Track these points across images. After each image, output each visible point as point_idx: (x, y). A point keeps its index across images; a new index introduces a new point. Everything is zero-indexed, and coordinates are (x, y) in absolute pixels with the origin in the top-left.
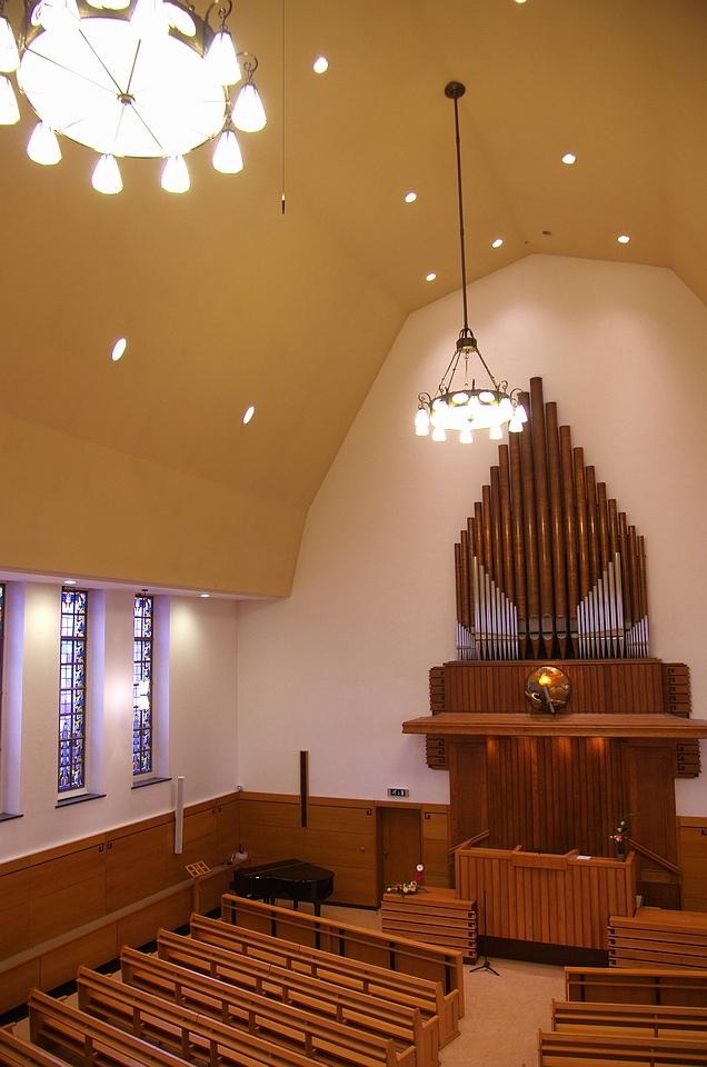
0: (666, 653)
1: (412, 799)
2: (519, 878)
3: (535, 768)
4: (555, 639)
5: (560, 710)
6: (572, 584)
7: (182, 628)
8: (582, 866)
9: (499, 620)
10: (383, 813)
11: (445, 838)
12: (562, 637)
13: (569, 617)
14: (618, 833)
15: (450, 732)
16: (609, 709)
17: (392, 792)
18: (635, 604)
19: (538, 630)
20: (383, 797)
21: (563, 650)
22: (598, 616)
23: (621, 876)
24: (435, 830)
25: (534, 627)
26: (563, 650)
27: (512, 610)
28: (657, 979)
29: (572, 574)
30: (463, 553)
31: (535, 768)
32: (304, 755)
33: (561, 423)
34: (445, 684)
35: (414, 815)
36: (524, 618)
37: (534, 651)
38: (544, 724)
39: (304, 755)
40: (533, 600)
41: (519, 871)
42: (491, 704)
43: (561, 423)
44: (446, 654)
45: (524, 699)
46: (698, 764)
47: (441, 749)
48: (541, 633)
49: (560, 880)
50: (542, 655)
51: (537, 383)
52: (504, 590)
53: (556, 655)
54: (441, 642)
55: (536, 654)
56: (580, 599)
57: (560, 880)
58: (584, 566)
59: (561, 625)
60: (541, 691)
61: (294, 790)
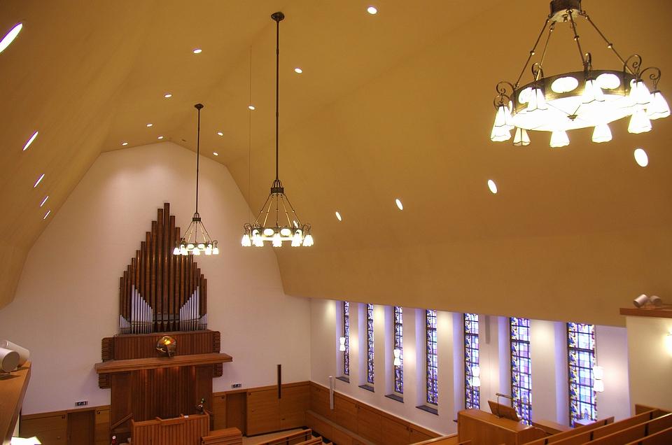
0: (212, 327)
1: (243, 388)
2: (164, 431)
3: (146, 381)
4: (162, 324)
5: (173, 354)
6: (177, 299)
7: (379, 316)
8: (186, 420)
9: (143, 313)
10: (70, 415)
11: (108, 421)
12: (172, 322)
13: (177, 314)
14: (201, 404)
15: (123, 370)
16: (192, 353)
17: (78, 404)
18: (203, 310)
19: (161, 319)
20: (72, 407)
21: (171, 328)
22: (188, 312)
23: (206, 421)
24: (103, 420)
25: (159, 318)
26: (171, 328)
27: (151, 311)
28: (288, 438)
29: (177, 294)
30: (127, 284)
31: (146, 381)
32: (279, 367)
33: (176, 226)
34: (111, 348)
35: (92, 413)
36: (155, 314)
37: (158, 328)
38: (165, 362)
39: (279, 367)
40: (159, 305)
41: (164, 429)
42: (139, 354)
43: (176, 226)
44: (112, 332)
45: (153, 350)
46: (222, 371)
47: (105, 379)
48: (162, 321)
49: (167, 429)
50: (162, 330)
51: (167, 205)
52: (145, 299)
53: (168, 330)
54: (110, 326)
55: (165, 329)
56: (180, 307)
57: (182, 428)
58: (182, 291)
59: (172, 317)
60: (165, 347)
61: (275, 383)
